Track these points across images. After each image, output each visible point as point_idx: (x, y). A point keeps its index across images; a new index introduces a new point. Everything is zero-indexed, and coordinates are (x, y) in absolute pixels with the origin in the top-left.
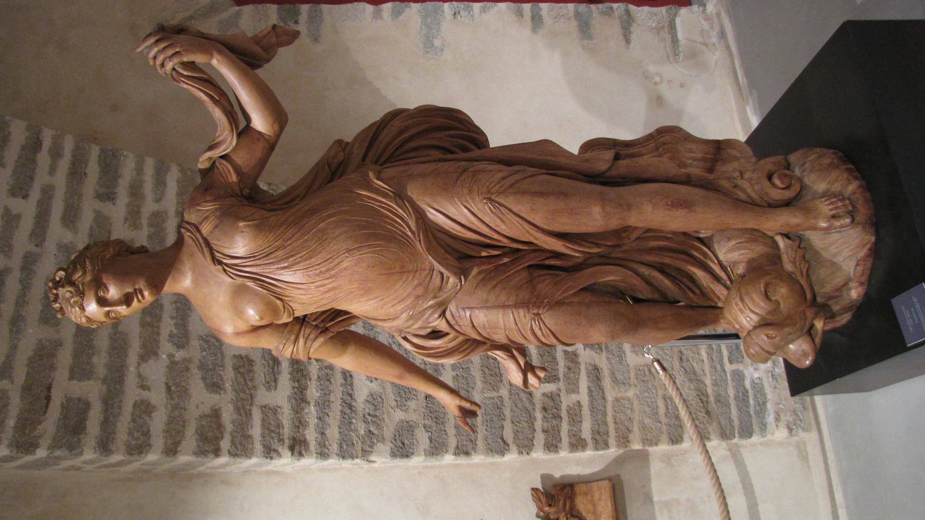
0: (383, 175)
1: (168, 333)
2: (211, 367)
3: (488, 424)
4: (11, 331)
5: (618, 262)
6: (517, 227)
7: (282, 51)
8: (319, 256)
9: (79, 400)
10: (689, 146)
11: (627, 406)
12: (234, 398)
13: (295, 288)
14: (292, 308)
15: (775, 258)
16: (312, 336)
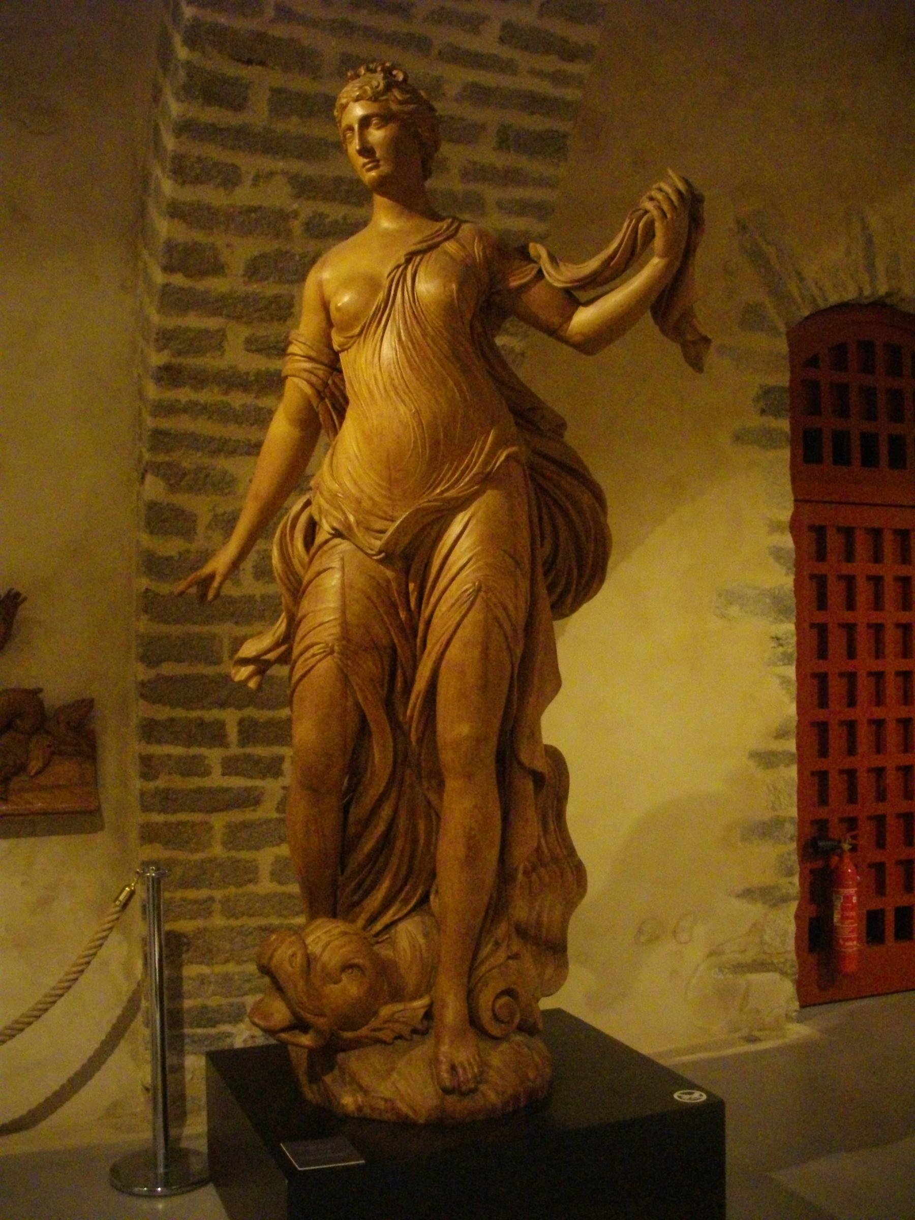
0: (513, 464)
2: (281, 265)
4: (334, 21)
7: (675, 349)
9: (245, 99)
13: (375, 350)
14: (350, 348)
15: (397, 995)
16: (314, 379)
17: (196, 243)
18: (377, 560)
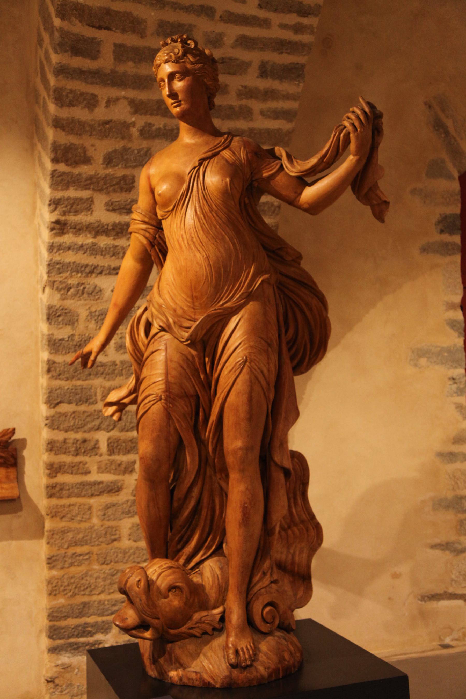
1: (153, 123)
2: (125, 157)
3: (73, 391)
5: (202, 471)
6: (226, 383)
8: (204, 237)
10: (305, 551)
11: (84, 516)
12: (100, 175)
14: (167, 217)
16: (147, 235)
17: (72, 144)
18: (186, 345)
